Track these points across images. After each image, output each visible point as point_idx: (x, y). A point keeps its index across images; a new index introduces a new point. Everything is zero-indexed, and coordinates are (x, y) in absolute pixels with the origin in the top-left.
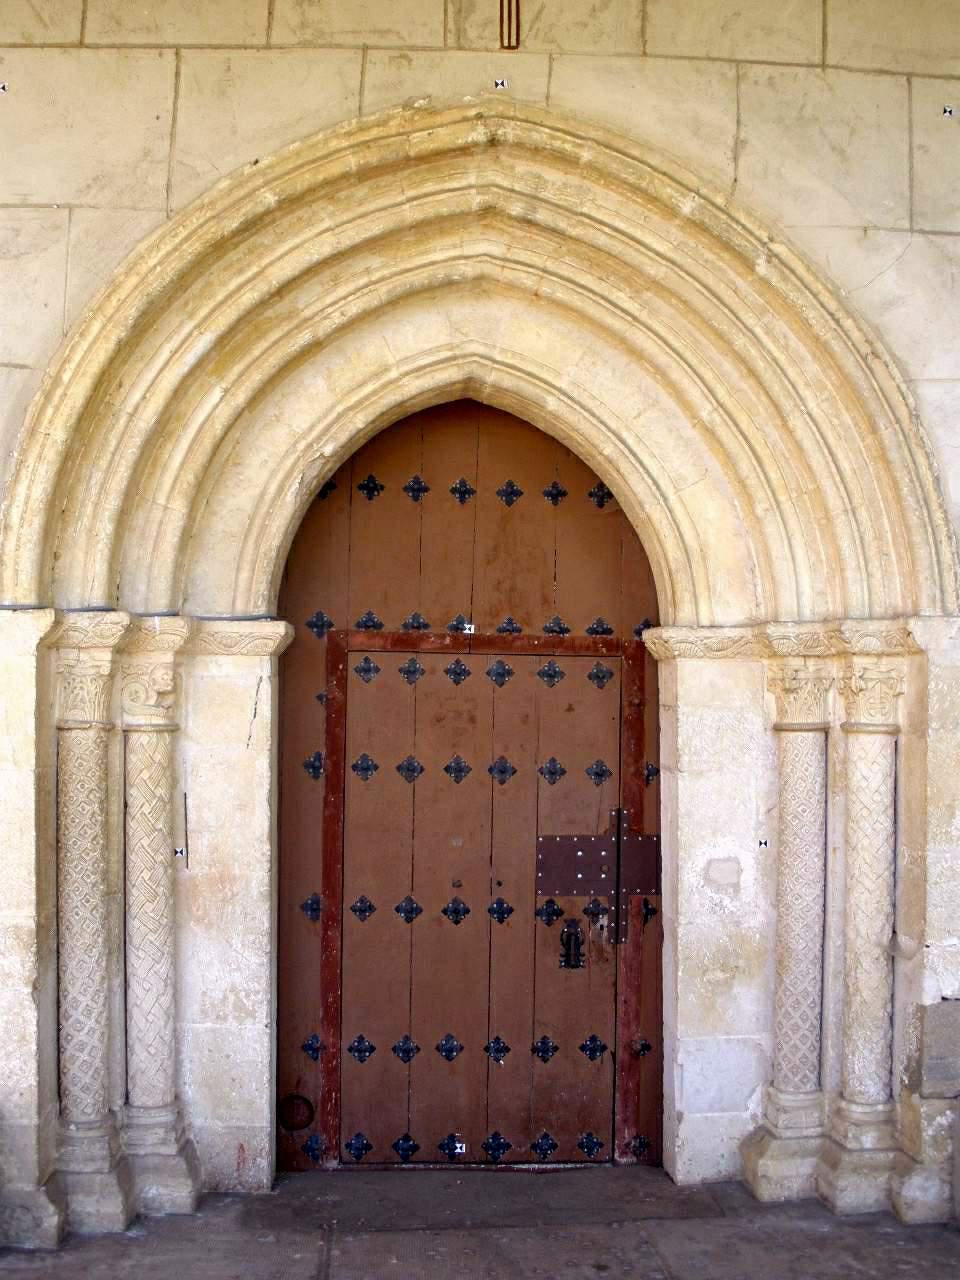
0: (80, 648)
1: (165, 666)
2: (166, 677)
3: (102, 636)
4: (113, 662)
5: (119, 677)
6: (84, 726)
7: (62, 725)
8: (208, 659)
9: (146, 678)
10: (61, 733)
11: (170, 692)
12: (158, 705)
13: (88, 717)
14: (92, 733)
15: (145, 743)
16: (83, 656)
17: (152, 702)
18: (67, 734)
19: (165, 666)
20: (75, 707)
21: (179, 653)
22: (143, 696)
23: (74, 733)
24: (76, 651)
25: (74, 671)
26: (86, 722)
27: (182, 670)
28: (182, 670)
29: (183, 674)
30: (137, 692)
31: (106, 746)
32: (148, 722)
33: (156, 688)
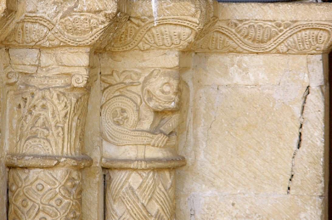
0: (41, 48)
1: (166, 72)
2: (167, 89)
3: (74, 30)
4: (91, 67)
5: (97, 87)
6: (48, 163)
7: (15, 161)
8: (227, 59)
9: (137, 89)
10: (12, 172)
11: (173, 111)
12: (154, 130)
13: (54, 150)
14: (59, 173)
15: (135, 187)
16: (46, 60)
17: (146, 125)
18: (22, 175)
19: (166, 72)
20: (34, 136)
21: (185, 52)
22: (132, 117)
23: (33, 174)
24: (35, 52)
25: (34, 81)
26: (52, 158)
27: (187, 77)
28: (187, 77)
29: (190, 84)
30: (123, 111)
31: (80, 192)
32: (141, 155)
33: (152, 104)
